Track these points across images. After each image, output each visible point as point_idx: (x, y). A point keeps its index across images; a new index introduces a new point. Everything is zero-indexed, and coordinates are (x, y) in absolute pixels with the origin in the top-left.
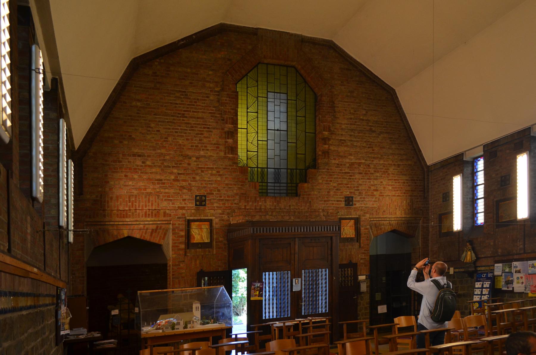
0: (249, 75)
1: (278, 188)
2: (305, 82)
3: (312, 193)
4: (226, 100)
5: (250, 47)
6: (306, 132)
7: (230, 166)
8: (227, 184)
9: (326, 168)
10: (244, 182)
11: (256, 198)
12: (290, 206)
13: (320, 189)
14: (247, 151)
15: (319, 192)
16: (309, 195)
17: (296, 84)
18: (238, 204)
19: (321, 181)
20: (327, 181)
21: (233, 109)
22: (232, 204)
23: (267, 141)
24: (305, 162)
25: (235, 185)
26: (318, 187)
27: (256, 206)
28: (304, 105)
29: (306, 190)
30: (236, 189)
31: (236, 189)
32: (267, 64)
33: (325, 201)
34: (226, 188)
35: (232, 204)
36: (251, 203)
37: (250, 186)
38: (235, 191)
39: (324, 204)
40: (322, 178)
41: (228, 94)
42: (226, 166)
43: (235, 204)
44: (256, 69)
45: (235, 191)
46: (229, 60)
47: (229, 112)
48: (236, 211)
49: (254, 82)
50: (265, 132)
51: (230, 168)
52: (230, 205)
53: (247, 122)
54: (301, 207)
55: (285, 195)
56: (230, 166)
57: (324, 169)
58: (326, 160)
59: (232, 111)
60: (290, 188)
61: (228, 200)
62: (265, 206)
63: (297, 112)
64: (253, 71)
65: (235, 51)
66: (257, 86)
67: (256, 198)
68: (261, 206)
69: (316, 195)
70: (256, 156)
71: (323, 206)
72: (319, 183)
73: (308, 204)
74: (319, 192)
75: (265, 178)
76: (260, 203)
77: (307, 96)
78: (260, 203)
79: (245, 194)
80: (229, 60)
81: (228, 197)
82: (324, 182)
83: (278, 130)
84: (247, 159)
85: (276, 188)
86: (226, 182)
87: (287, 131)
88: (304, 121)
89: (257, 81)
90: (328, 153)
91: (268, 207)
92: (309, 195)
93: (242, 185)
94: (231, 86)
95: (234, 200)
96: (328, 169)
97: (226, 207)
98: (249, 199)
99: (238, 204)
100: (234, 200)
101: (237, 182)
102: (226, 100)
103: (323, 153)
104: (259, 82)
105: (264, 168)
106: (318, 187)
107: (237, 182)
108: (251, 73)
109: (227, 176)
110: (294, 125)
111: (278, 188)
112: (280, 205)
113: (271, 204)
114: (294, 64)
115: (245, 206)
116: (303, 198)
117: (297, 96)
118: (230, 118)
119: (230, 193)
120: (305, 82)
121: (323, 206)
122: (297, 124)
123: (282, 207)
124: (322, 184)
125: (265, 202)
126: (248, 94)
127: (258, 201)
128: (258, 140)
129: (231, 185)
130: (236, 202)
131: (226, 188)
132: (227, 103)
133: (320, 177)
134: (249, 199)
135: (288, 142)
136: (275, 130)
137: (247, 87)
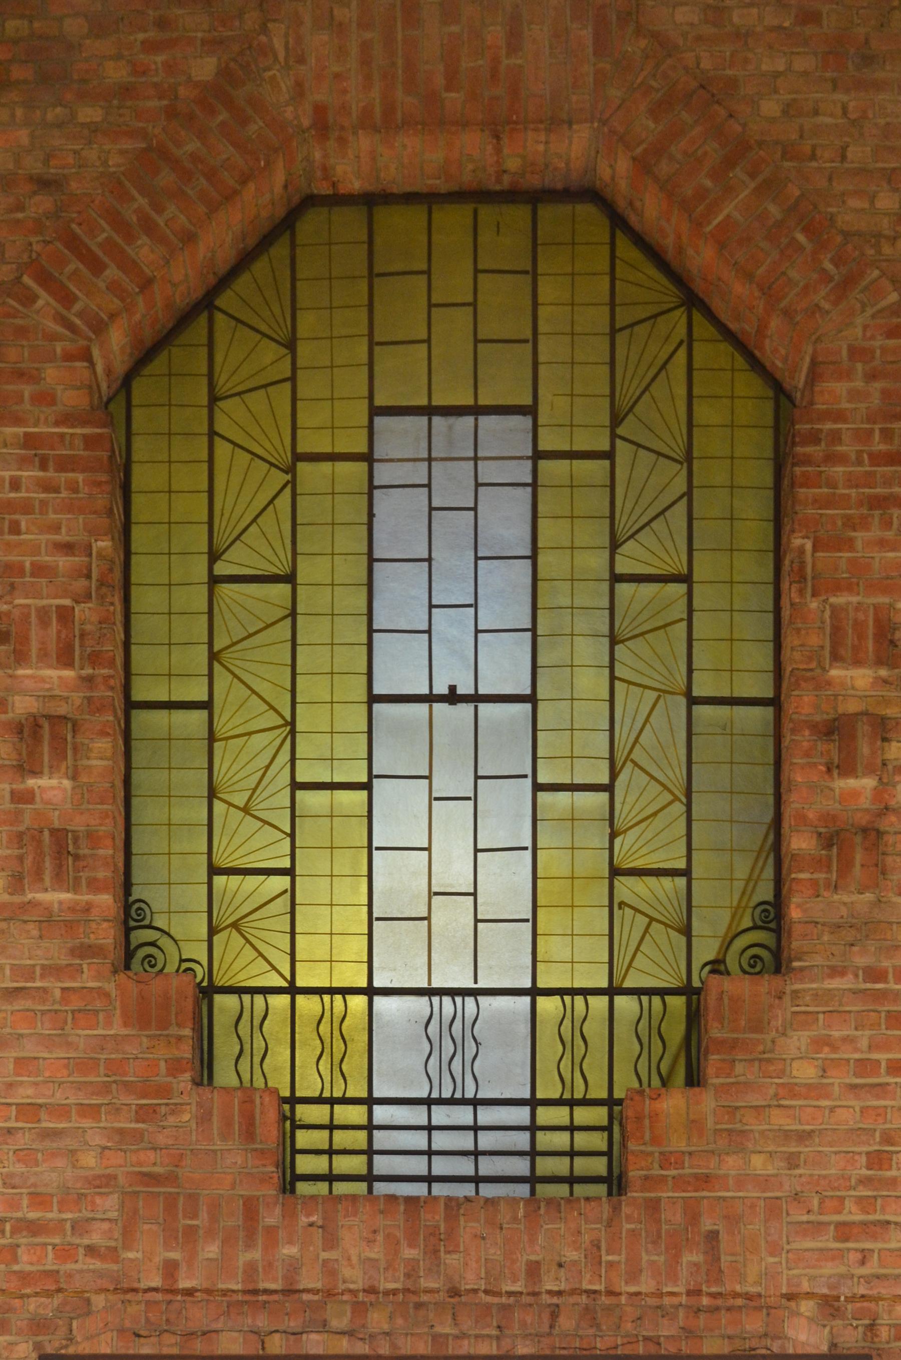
0: (224, 300)
1: (418, 1140)
2: (693, 300)
3: (731, 1165)
4: (15, 485)
5: (205, 68)
6: (693, 701)
7: (49, 971)
8: (29, 1111)
9: (861, 961)
10: (164, 1091)
11: (251, 1210)
12: (534, 1270)
13: (804, 1137)
14: (214, 870)
15: (792, 1161)
16: (705, 1180)
17: (613, 332)
18: (112, 1254)
19: (805, 1072)
20: (865, 1066)
21: (68, 548)
22: (65, 1253)
23: (367, 787)
24: (687, 931)
25: (91, 1111)
26: (779, 1120)
27: (251, 1269)
28: (680, 485)
29: (678, 1143)
30: (98, 1140)
31: (98, 1140)
32: (372, 201)
33: (844, 1231)
34: (23, 1140)
35: (65, 1253)
36: (212, 1250)
37: (204, 1119)
38: (89, 1160)
39: (839, 1256)
40: (820, 1043)
41: (29, 441)
42: (28, 973)
43: (91, 1250)
44: (280, 250)
45: (89, 1160)
46: (44, 184)
47: (39, 570)
48: (99, 1301)
49: (270, 352)
50: (357, 718)
51: (55, 986)
52: (50, 1264)
53: (213, 656)
54: (633, 1275)
55: (601, 1190)
56: (49, 971)
57: (836, 972)
58: (854, 900)
59: (63, 562)
60: (561, 1140)
61: (34, 1228)
62: (330, 1270)
63: (614, 545)
64: (260, 267)
65: (90, 114)
66: (293, 379)
67: (251, 1210)
68: (293, 1268)
69: (764, 1182)
70: (283, 904)
71: (829, 1269)
72: (792, 1090)
73: (691, 1257)
74: (792, 1161)
75: (355, 1064)
76: (289, 1250)
77: (702, 412)
78: (289, 1250)
79: (170, 1179)
80: (44, 184)
81: (39, 1199)
82: (837, 1080)
83: (453, 697)
84: (212, 931)
85: (441, 1141)
86: (25, 1094)
87: (532, 699)
88: (680, 610)
89: (291, 345)
90: (872, 834)
91: (353, 1276)
92: (705, 1180)
93: (144, 1114)
94: (51, 374)
95: (78, 1227)
96: (875, 974)
97: (24, 1277)
98: (202, 1220)
99: (112, 1254)
100: (78, 1227)
101: (105, 1088)
102: (15, 485)
103: (827, 842)
104: (303, 349)
105: (345, 991)
106: (779, 1120)
107: (105, 1088)
108: (243, 283)
109: (29, 1049)
110: (591, 650)
111: (465, 1141)
112: (452, 1260)
113: (376, 1252)
114: (571, 150)
115: (170, 1269)
116: (654, 1206)
117: (616, 420)
118: (43, 615)
119: (51, 1175)
120: (693, 300)
121: (829, 1269)
122: (614, 641)
123: (471, 1279)
124: (816, 1090)
125: (331, 1242)
126: (222, 449)
127: (271, 1231)
128: (296, 786)
129: (62, 1111)
130: (95, 1238)
131: (23, 1140)
132: (26, 508)
133: (798, 1041)
134: (202, 1220)
135: (537, 787)
136: (430, 698)
137: (214, 399)
